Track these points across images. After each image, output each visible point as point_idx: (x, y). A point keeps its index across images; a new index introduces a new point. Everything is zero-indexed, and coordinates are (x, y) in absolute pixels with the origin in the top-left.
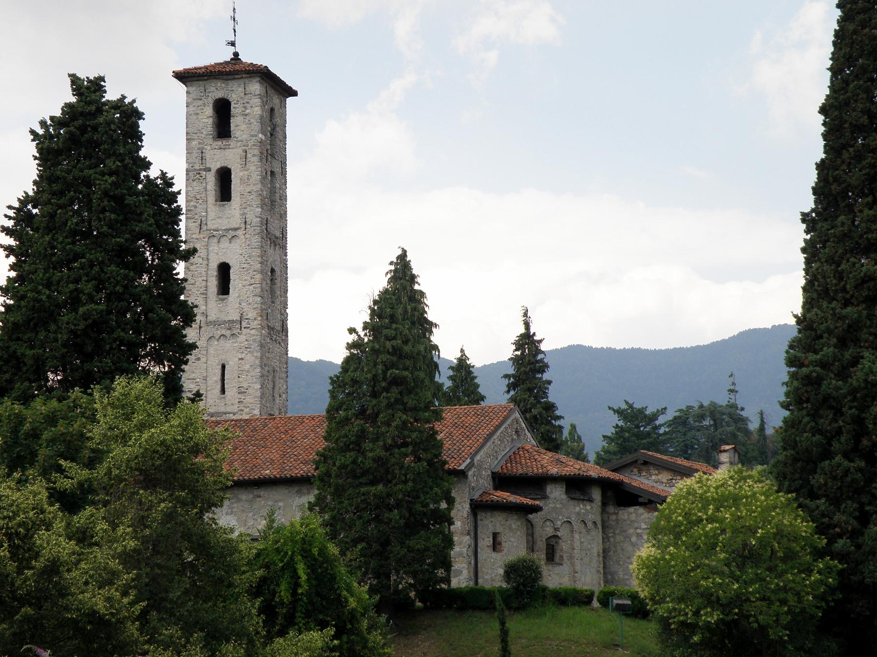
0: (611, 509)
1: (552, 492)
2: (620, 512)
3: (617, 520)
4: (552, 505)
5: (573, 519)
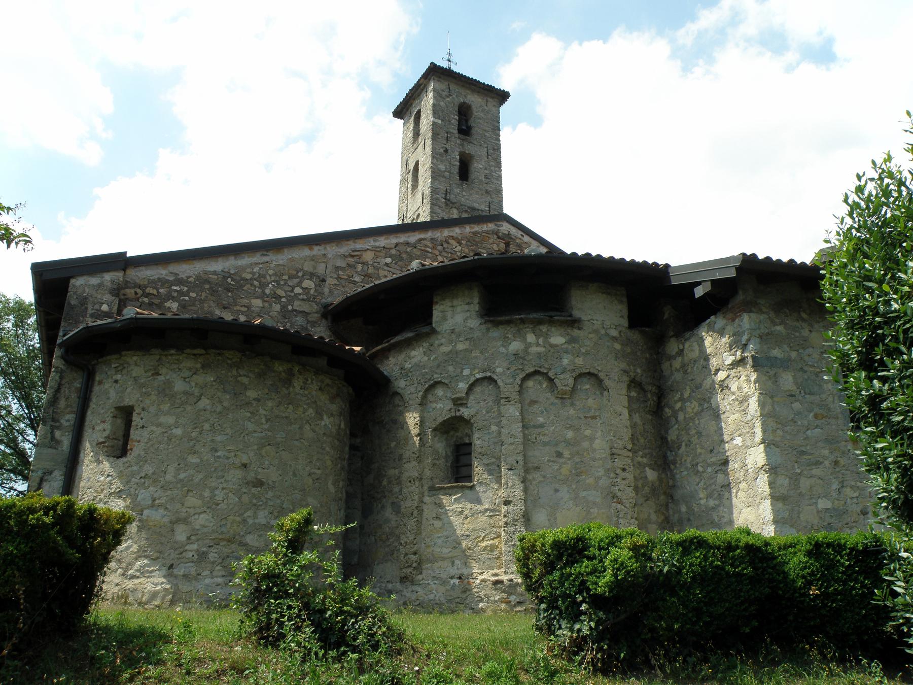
1: (444, 319)
4: (445, 349)
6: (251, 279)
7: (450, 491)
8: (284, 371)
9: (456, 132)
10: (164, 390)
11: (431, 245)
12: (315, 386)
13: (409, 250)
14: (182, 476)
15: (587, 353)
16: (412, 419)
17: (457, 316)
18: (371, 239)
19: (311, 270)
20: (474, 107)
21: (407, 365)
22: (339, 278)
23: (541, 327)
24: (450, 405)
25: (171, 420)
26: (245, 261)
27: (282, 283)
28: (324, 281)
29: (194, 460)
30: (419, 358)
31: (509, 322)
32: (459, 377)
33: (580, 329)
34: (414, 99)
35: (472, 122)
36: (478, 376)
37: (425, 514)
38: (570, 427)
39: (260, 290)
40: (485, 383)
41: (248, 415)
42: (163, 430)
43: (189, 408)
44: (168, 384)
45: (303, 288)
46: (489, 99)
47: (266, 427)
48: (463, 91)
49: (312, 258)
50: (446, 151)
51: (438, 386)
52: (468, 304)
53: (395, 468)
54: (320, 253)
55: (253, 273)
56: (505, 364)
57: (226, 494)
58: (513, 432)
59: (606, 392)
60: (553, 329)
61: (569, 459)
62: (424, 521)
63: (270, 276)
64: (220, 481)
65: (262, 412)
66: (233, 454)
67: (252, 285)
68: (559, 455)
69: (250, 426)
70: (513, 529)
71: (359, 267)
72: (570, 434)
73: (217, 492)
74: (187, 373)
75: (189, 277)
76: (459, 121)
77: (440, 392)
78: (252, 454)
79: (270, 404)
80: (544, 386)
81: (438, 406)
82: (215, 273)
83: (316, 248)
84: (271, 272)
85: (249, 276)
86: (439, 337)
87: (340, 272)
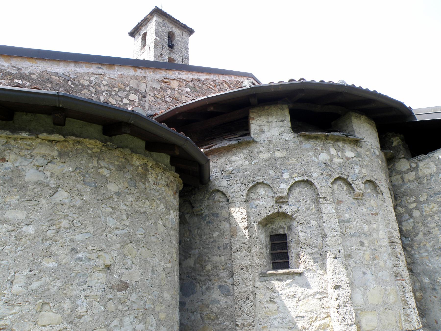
0: (403, 164)
1: (262, 131)
2: (421, 164)
3: (418, 179)
4: (263, 156)
5: (315, 175)
6: (88, 86)
7: (281, 277)
8: (141, 166)
9: (167, 46)
10: (11, 179)
11: (213, 84)
12: (163, 182)
13: (200, 85)
14: (35, 285)
15: (367, 166)
16: (238, 214)
17: (271, 129)
18: (177, 72)
19: (135, 87)
20: (176, 34)
21: (227, 167)
22: (155, 97)
23: (339, 143)
24: (272, 203)
25: (20, 215)
26: (83, 69)
27: (113, 93)
28: (144, 97)
29: (50, 264)
30: (240, 162)
31: (316, 138)
32: (280, 179)
33: (361, 147)
34: (142, 26)
35: (174, 42)
36: (297, 179)
37: (258, 297)
38: (365, 222)
39: (96, 96)
40: (302, 185)
41: (110, 210)
42: (10, 228)
43: (43, 201)
44: (18, 172)
45: (130, 100)
46: (184, 32)
47: (127, 223)
48: (171, 26)
49: (137, 78)
50: (162, 55)
51: (259, 186)
52: (282, 121)
53: (220, 256)
54: (141, 75)
55: (90, 82)
56: (319, 170)
57: (90, 304)
58: (333, 226)
59: (380, 195)
60: (346, 146)
61: (368, 247)
62: (258, 304)
63: (104, 85)
64: (82, 288)
65: (123, 207)
66: (95, 255)
67: (89, 90)
68: (362, 244)
69: (112, 223)
70: (345, 310)
71: (169, 91)
72: (366, 228)
73: (79, 302)
74: (41, 161)
75: (31, 74)
76: (168, 40)
77: (261, 191)
78: (115, 254)
79: (130, 199)
80: (345, 189)
81: (261, 203)
82: (56, 74)
83: (139, 71)
84: (104, 83)
85: (86, 83)
86: (258, 146)
87: (156, 93)
